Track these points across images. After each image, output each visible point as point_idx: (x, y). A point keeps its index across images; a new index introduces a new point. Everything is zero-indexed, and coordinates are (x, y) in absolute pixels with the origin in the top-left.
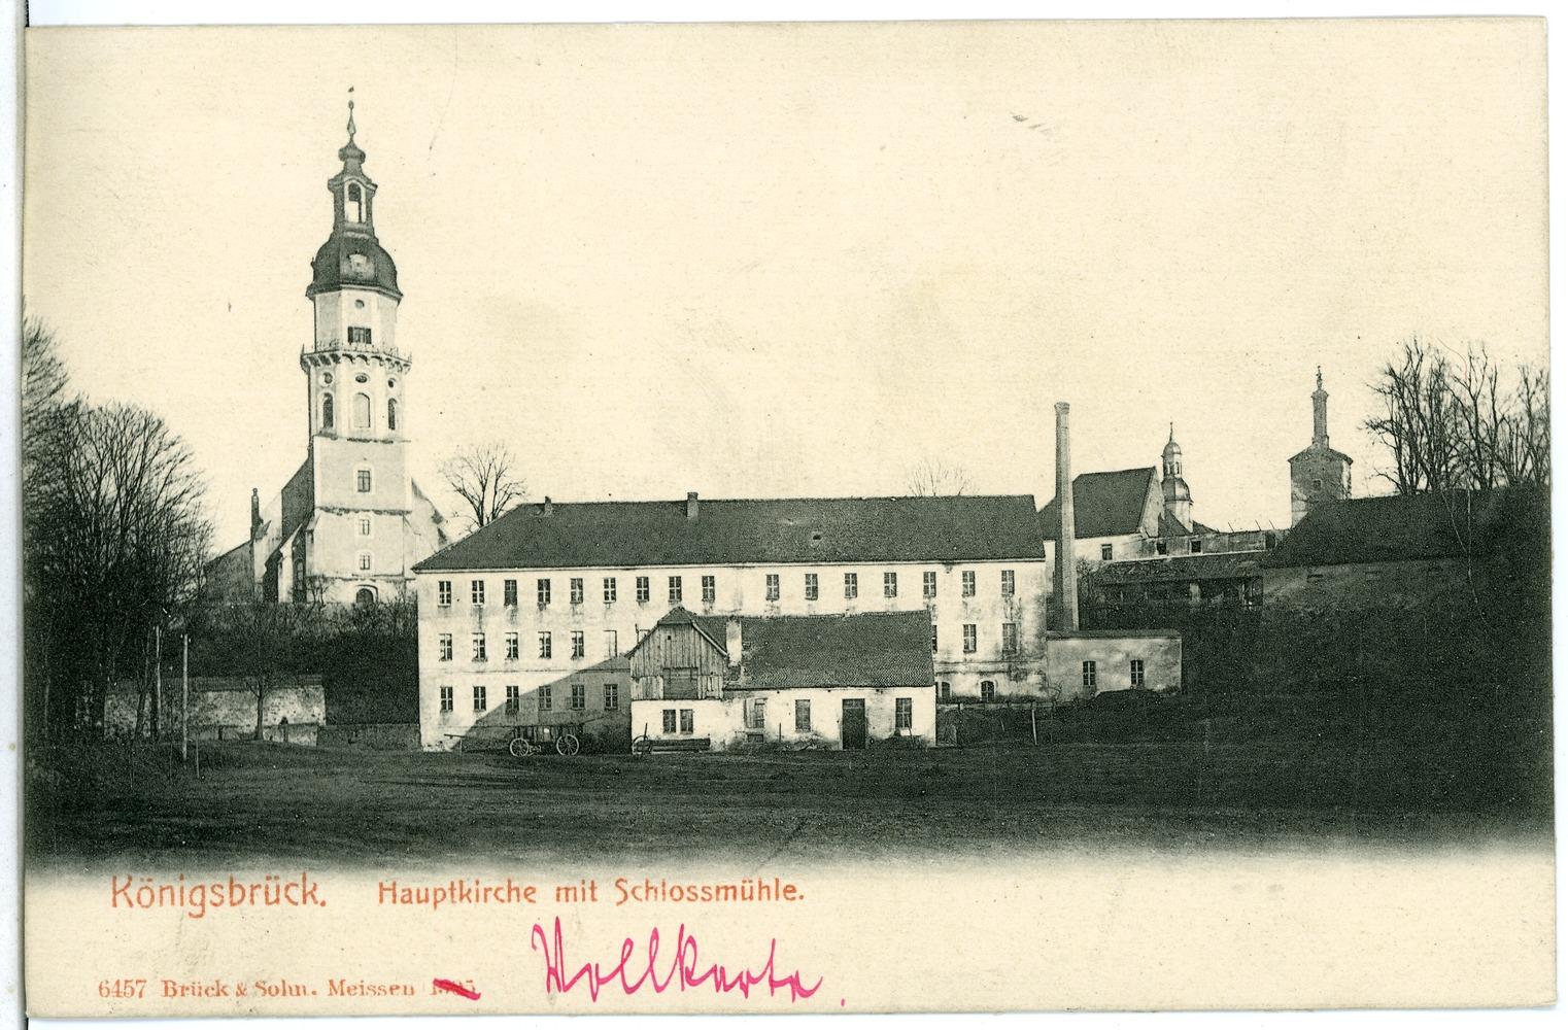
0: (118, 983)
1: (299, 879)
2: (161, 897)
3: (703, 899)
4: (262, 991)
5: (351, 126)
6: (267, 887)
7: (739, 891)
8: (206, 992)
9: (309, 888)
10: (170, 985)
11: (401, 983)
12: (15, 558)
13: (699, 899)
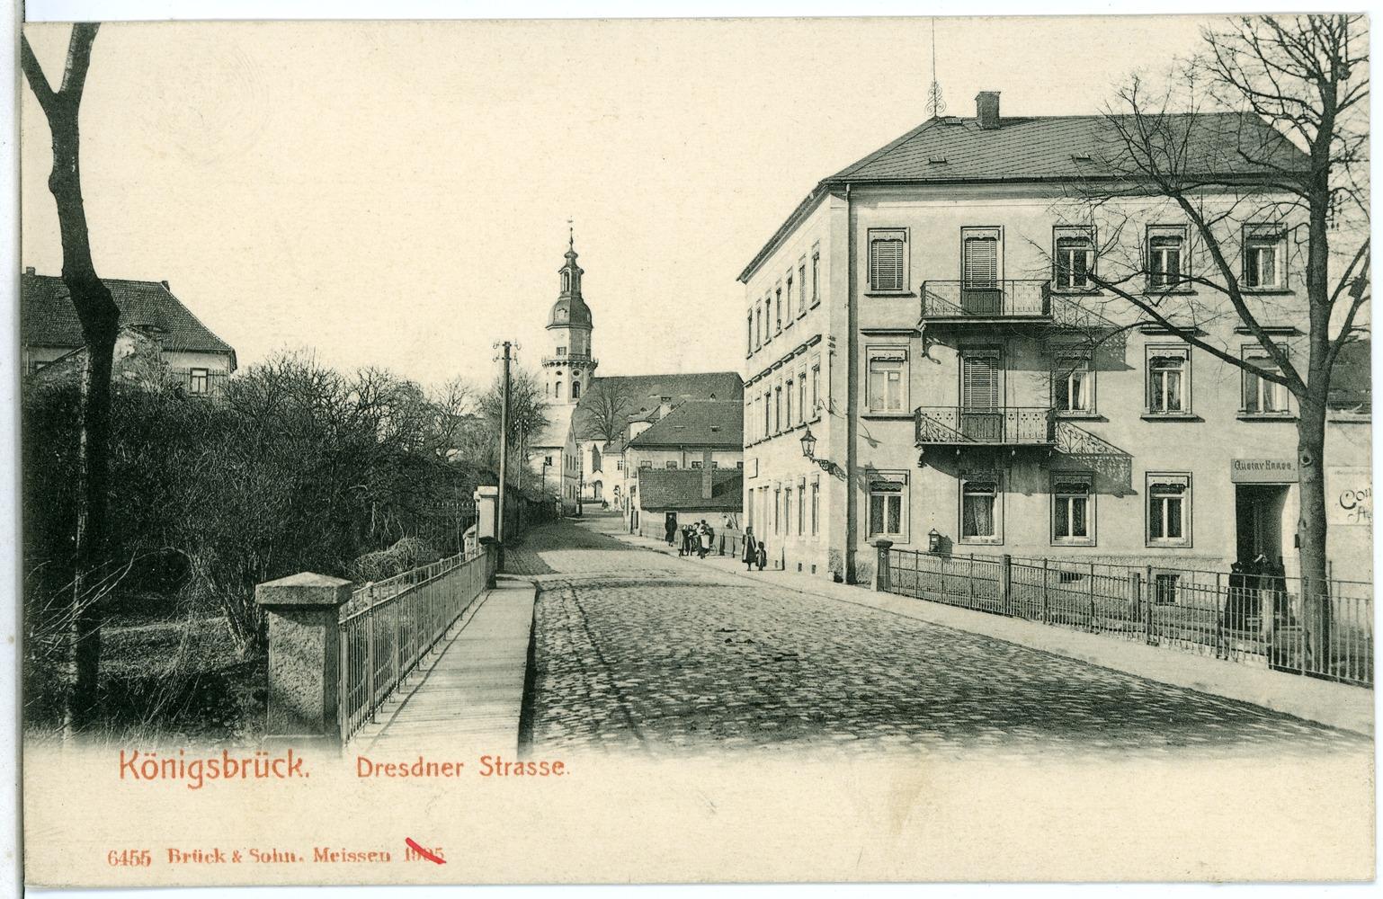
0: (125, 853)
1: (284, 754)
2: (163, 769)
3: (541, 773)
4: (256, 858)
5: (572, 242)
6: (257, 762)
7: (178, 766)
8: (207, 857)
9: (295, 763)
10: (175, 853)
11: (377, 850)
12: (13, 473)
13: (538, 774)
